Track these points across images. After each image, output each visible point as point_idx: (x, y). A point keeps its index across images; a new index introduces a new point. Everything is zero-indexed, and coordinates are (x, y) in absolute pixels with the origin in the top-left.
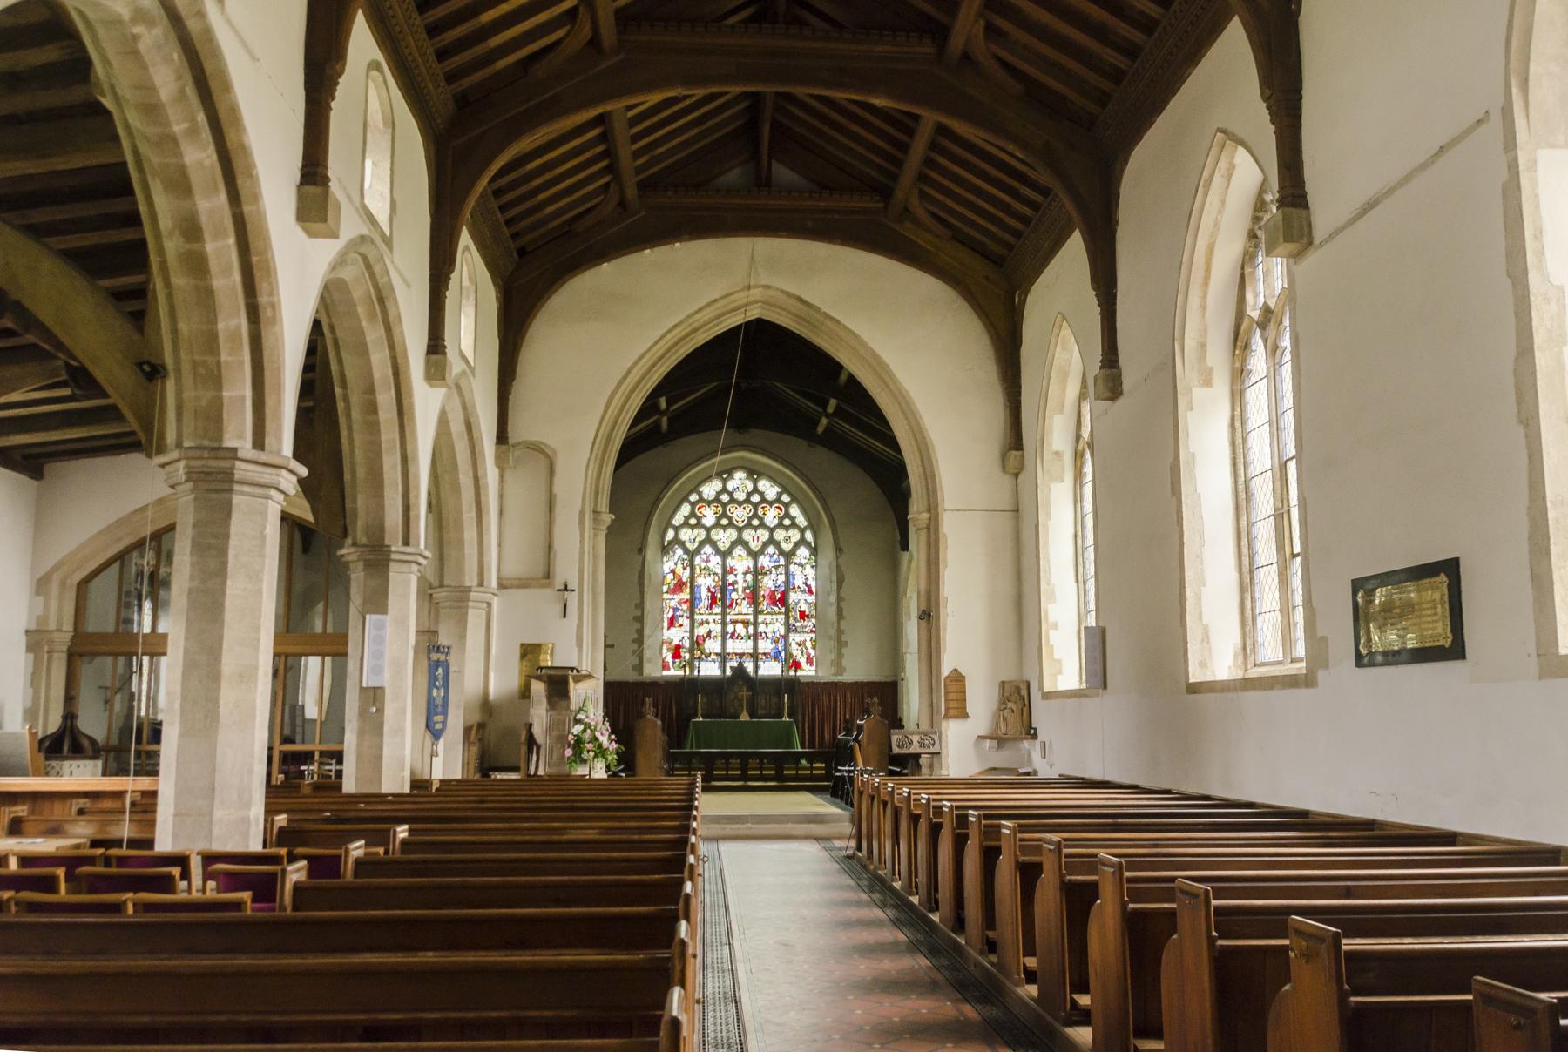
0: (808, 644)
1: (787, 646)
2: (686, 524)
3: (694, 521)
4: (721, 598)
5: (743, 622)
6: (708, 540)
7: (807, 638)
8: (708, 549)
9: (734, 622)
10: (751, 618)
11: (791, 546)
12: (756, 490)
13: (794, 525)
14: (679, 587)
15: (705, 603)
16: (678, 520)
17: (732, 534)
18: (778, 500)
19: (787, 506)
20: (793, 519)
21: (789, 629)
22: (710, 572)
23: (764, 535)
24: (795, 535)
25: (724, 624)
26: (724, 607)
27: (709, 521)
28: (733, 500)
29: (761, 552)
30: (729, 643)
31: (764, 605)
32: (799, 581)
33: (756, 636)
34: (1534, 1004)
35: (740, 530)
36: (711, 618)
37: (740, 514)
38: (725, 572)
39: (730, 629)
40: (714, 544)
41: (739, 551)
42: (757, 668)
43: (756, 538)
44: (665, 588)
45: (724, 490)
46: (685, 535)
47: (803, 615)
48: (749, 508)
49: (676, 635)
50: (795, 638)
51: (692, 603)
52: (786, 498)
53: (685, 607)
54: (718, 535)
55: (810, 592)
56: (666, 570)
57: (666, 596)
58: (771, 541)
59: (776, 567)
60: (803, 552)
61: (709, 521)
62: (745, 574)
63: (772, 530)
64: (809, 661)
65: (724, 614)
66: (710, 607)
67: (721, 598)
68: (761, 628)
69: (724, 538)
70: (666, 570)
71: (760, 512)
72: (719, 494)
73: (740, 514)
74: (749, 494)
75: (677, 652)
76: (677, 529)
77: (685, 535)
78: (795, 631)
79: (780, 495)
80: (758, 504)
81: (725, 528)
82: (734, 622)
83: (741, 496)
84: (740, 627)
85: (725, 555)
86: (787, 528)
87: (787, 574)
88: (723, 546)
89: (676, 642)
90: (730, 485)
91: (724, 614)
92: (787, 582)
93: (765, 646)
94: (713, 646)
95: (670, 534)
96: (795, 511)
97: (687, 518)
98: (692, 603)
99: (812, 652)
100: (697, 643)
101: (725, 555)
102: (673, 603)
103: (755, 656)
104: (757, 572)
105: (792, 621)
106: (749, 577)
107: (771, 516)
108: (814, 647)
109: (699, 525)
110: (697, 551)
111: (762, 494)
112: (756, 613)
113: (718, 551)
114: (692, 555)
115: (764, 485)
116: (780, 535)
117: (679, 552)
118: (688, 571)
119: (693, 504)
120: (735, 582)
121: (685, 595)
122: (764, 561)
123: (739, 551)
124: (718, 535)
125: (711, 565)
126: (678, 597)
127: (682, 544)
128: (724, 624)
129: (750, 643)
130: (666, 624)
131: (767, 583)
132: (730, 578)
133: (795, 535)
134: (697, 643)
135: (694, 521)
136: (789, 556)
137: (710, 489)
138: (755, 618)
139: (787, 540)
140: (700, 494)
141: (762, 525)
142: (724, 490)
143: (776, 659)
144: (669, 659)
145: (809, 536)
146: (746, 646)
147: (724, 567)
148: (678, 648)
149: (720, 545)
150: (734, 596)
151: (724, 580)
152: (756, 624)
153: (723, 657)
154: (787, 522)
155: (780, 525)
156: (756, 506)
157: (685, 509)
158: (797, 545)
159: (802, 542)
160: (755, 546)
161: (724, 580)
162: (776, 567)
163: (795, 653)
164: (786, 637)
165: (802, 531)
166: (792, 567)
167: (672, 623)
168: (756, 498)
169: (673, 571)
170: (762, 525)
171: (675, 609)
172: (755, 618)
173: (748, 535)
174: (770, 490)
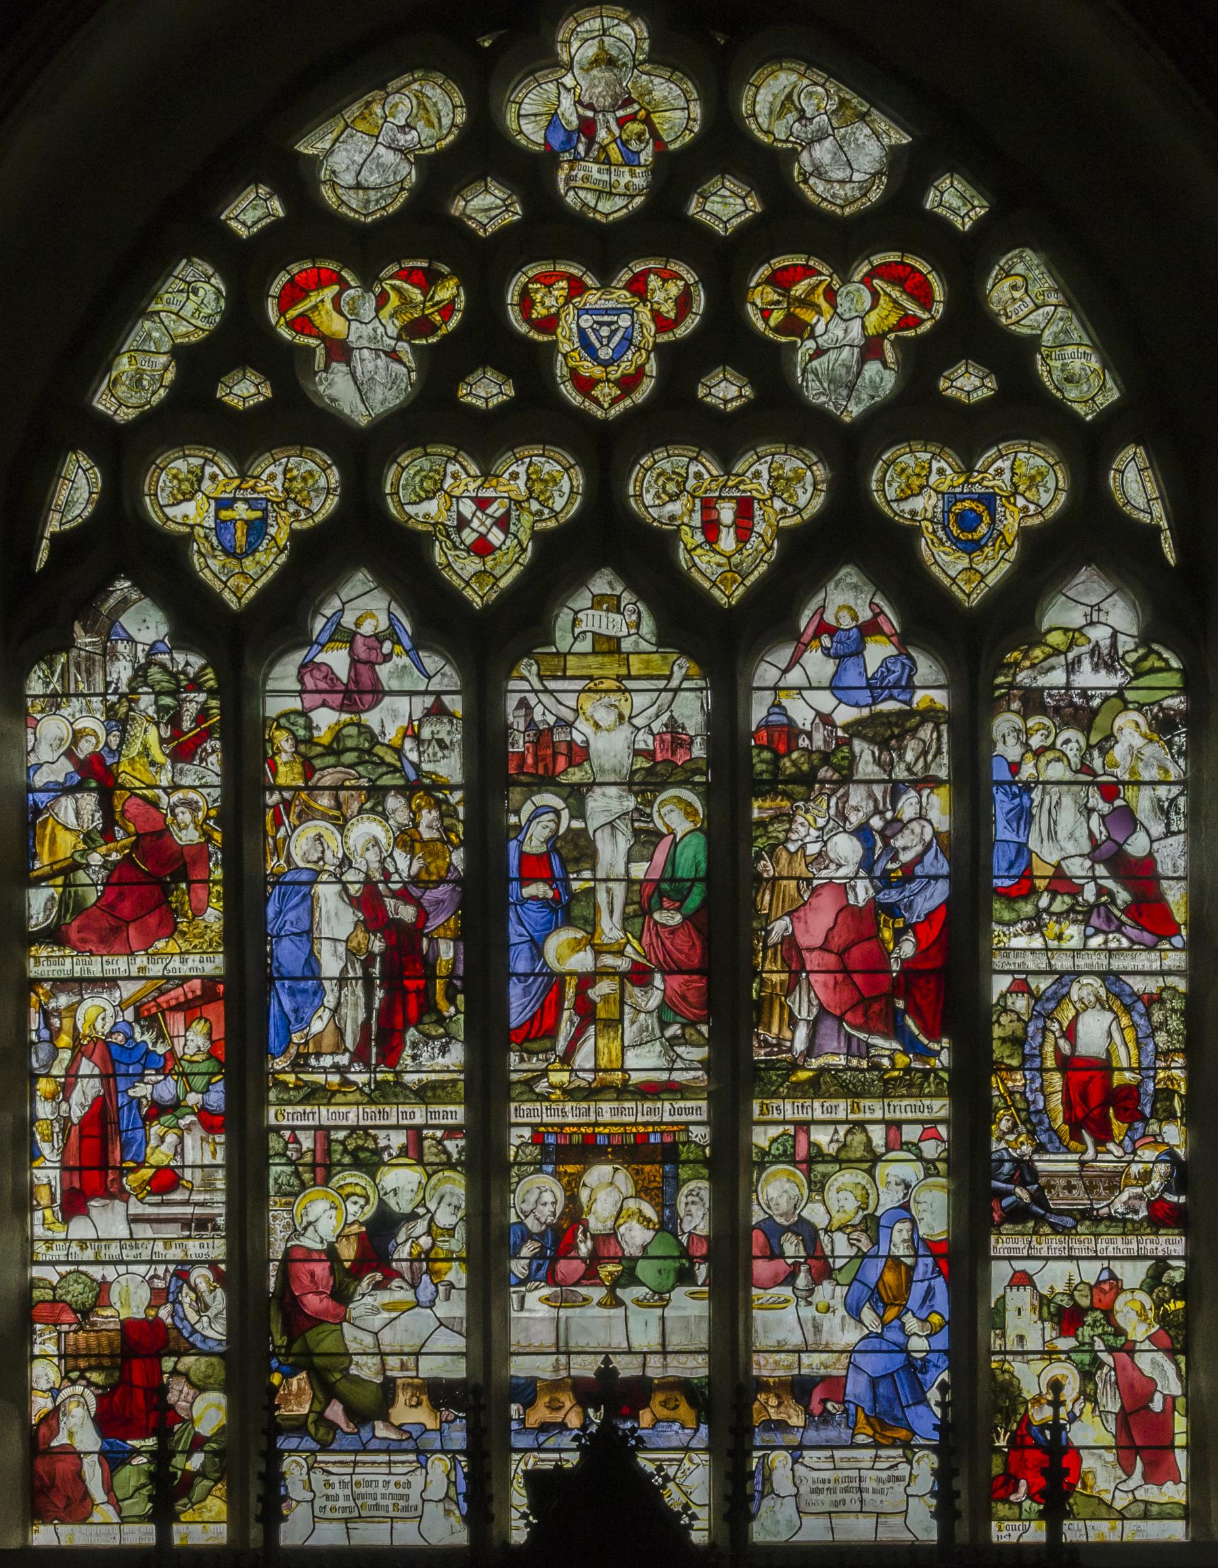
0: (1135, 1317)
1: (970, 1318)
2: (190, 412)
3: (249, 391)
4: (458, 966)
5: (632, 1151)
6: (359, 535)
7: (1129, 1267)
8: (363, 603)
9: (570, 1153)
10: (692, 1117)
11: (996, 567)
12: (725, 144)
13: (1022, 407)
14: (146, 887)
15: (337, 1013)
16: (133, 382)
17: (545, 483)
18: (897, 218)
19: (967, 259)
20: (1012, 356)
21: (987, 1196)
22: (377, 777)
23: (793, 485)
24: (1029, 482)
25: (487, 1168)
26: (489, 1038)
27: (367, 379)
28: (552, 230)
29: (771, 612)
30: (532, 1311)
31: (797, 1025)
32: (1062, 837)
33: (729, 1265)
34: (508, 84)
35: (606, 451)
36: (392, 1126)
37: (604, 331)
38: (497, 768)
39: (536, 1198)
40: (402, 558)
41: (605, 612)
42: (737, 1492)
43: (722, 513)
44: (39, 904)
45: (485, 147)
46: (188, 496)
47: (1098, 1099)
48: (671, 286)
49: (118, 1256)
50: (1036, 1268)
51: (247, 1000)
52: (955, 201)
53: (193, 1040)
54: (435, 493)
55: (1149, 915)
56: (52, 768)
57: (45, 963)
58: (853, 533)
59: (887, 732)
60: (1095, 615)
61: (367, 379)
62: (647, 780)
63: (850, 450)
64: (1140, 1438)
65: (487, 1090)
66: (384, 1040)
67: (458, 966)
68: (777, 1191)
69: (481, 512)
70: (52, 768)
71: (762, 305)
72: (442, 173)
73: (604, 331)
74: (677, 174)
75: (133, 1371)
76: (126, 453)
77: (188, 496)
78: (1033, 1215)
79: (908, 174)
80: (474, 242)
81: (486, 438)
82: (570, 1153)
83: (604, 189)
84: (607, 1192)
85: (488, 640)
86: (967, 433)
87: (972, 781)
88: (477, 577)
89: (130, 1299)
90: (530, 114)
91: (487, 1090)
92: (969, 844)
93: (799, 1327)
94: (405, 1329)
95: (77, 490)
96: (1025, 294)
97: (199, 364)
98: (247, 1000)
99: (1164, 1376)
100: (276, 1319)
101: (488, 640)
102: (96, 1014)
103: (727, 1402)
104: (739, 773)
105: (1007, 1141)
106: (677, 814)
107: (845, 333)
108: (1178, 1337)
109: (298, 418)
110: (282, 616)
111: (769, 170)
112: (737, 1080)
113: (437, 614)
114: (237, 642)
115: (782, 99)
116: (914, 484)
117: (146, 625)
118: (207, 774)
119: (245, 266)
120: (577, 849)
121: (192, 956)
122: (800, 689)
123: (605, 612)
124: (435, 493)
125: (389, 718)
126: (135, 968)
127: (162, 565)
128: (487, 1168)
129: (691, 1308)
130: (47, 1174)
131: (823, 849)
132: (536, 823)
133: (1029, 482)
134: (276, 1319)
135: (249, 391)
136: (979, 642)
137: (367, 154)
138: (729, 1121)
139: (968, 522)
140: (297, 180)
141: (780, 412)
142: (485, 147)
143: (886, 1424)
144: (79, 1430)
145: (1135, 484)
146: (658, 1331)
147: (484, 736)
148: (145, 1344)
149: (459, 568)
150: (565, 952)
151: (485, 832)
152: (730, 1166)
153: (481, 1401)
154: (968, 383)
155: (916, 412)
156: (723, 264)
157: (190, 302)
158: (1049, 556)
159: (1084, 536)
160: (720, 566)
161: (485, 832)
162: (887, 732)
163: (1031, 1378)
164: (962, 1260)
165: (1087, 449)
166: (1006, 733)
167: (98, 1162)
168: (725, 206)
169: (96, 774)
170: (780, 412)
171: (117, 1060)
172: (729, 1121)
173: (664, 487)
174: (845, 152)
